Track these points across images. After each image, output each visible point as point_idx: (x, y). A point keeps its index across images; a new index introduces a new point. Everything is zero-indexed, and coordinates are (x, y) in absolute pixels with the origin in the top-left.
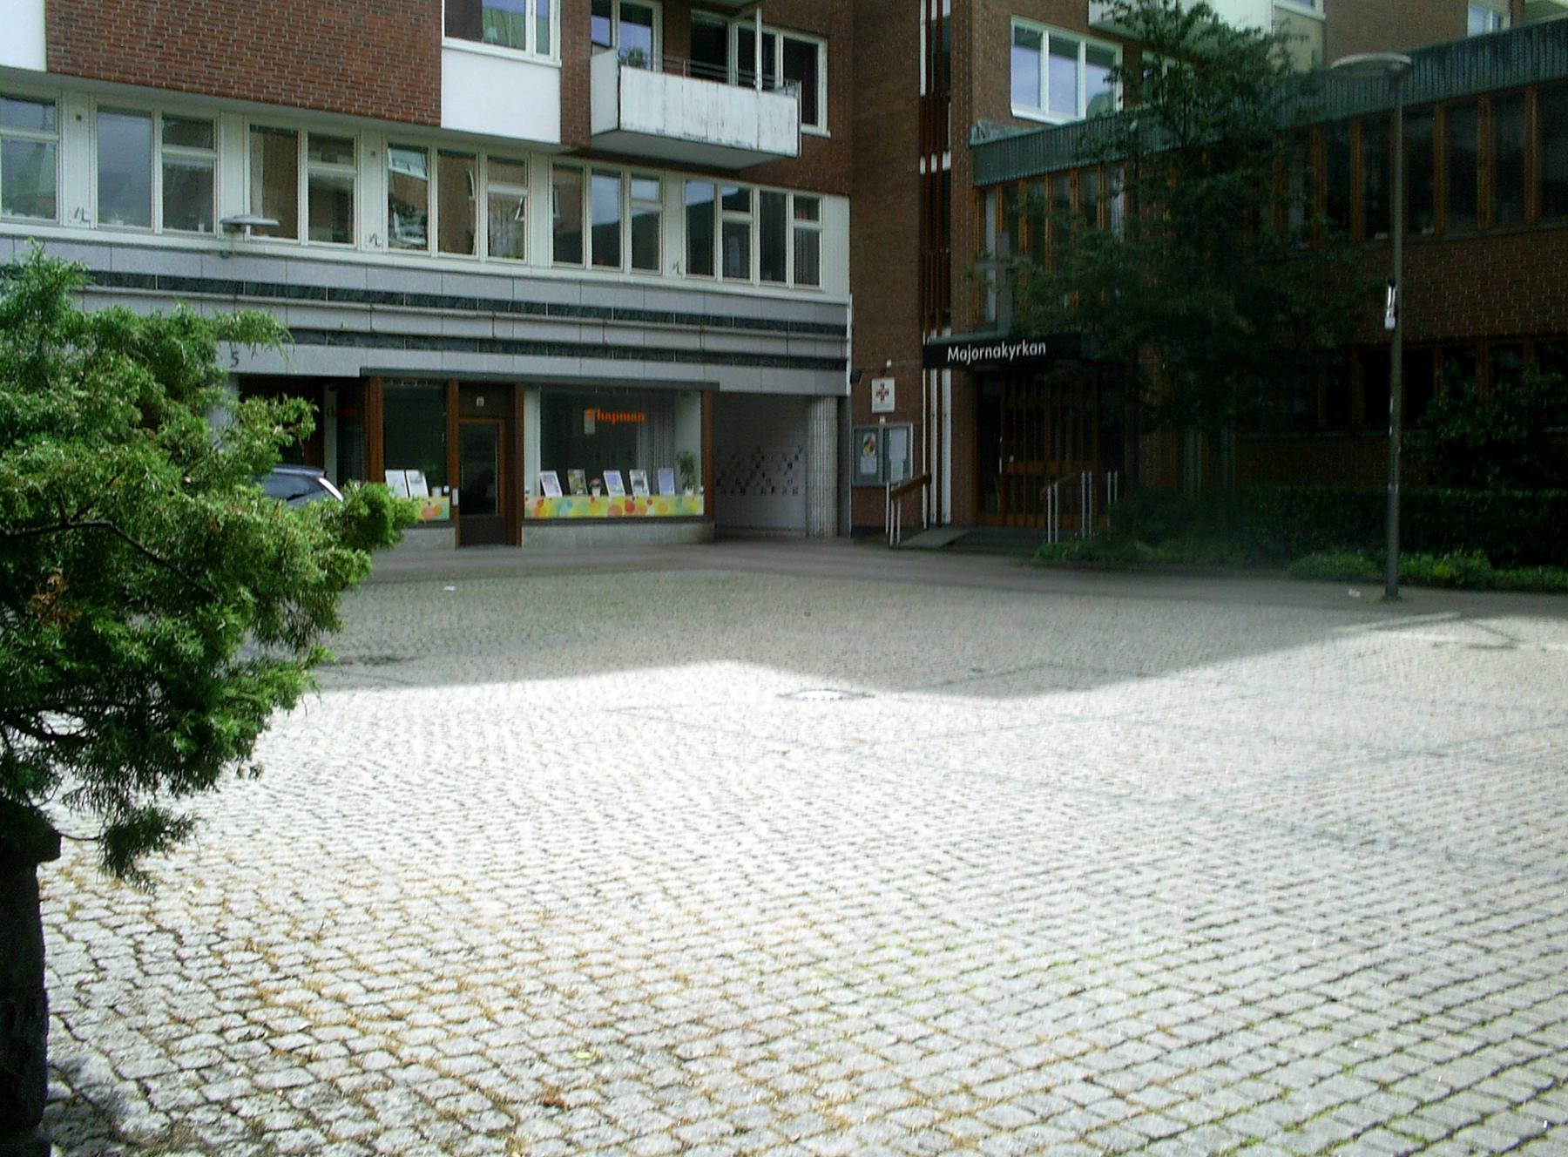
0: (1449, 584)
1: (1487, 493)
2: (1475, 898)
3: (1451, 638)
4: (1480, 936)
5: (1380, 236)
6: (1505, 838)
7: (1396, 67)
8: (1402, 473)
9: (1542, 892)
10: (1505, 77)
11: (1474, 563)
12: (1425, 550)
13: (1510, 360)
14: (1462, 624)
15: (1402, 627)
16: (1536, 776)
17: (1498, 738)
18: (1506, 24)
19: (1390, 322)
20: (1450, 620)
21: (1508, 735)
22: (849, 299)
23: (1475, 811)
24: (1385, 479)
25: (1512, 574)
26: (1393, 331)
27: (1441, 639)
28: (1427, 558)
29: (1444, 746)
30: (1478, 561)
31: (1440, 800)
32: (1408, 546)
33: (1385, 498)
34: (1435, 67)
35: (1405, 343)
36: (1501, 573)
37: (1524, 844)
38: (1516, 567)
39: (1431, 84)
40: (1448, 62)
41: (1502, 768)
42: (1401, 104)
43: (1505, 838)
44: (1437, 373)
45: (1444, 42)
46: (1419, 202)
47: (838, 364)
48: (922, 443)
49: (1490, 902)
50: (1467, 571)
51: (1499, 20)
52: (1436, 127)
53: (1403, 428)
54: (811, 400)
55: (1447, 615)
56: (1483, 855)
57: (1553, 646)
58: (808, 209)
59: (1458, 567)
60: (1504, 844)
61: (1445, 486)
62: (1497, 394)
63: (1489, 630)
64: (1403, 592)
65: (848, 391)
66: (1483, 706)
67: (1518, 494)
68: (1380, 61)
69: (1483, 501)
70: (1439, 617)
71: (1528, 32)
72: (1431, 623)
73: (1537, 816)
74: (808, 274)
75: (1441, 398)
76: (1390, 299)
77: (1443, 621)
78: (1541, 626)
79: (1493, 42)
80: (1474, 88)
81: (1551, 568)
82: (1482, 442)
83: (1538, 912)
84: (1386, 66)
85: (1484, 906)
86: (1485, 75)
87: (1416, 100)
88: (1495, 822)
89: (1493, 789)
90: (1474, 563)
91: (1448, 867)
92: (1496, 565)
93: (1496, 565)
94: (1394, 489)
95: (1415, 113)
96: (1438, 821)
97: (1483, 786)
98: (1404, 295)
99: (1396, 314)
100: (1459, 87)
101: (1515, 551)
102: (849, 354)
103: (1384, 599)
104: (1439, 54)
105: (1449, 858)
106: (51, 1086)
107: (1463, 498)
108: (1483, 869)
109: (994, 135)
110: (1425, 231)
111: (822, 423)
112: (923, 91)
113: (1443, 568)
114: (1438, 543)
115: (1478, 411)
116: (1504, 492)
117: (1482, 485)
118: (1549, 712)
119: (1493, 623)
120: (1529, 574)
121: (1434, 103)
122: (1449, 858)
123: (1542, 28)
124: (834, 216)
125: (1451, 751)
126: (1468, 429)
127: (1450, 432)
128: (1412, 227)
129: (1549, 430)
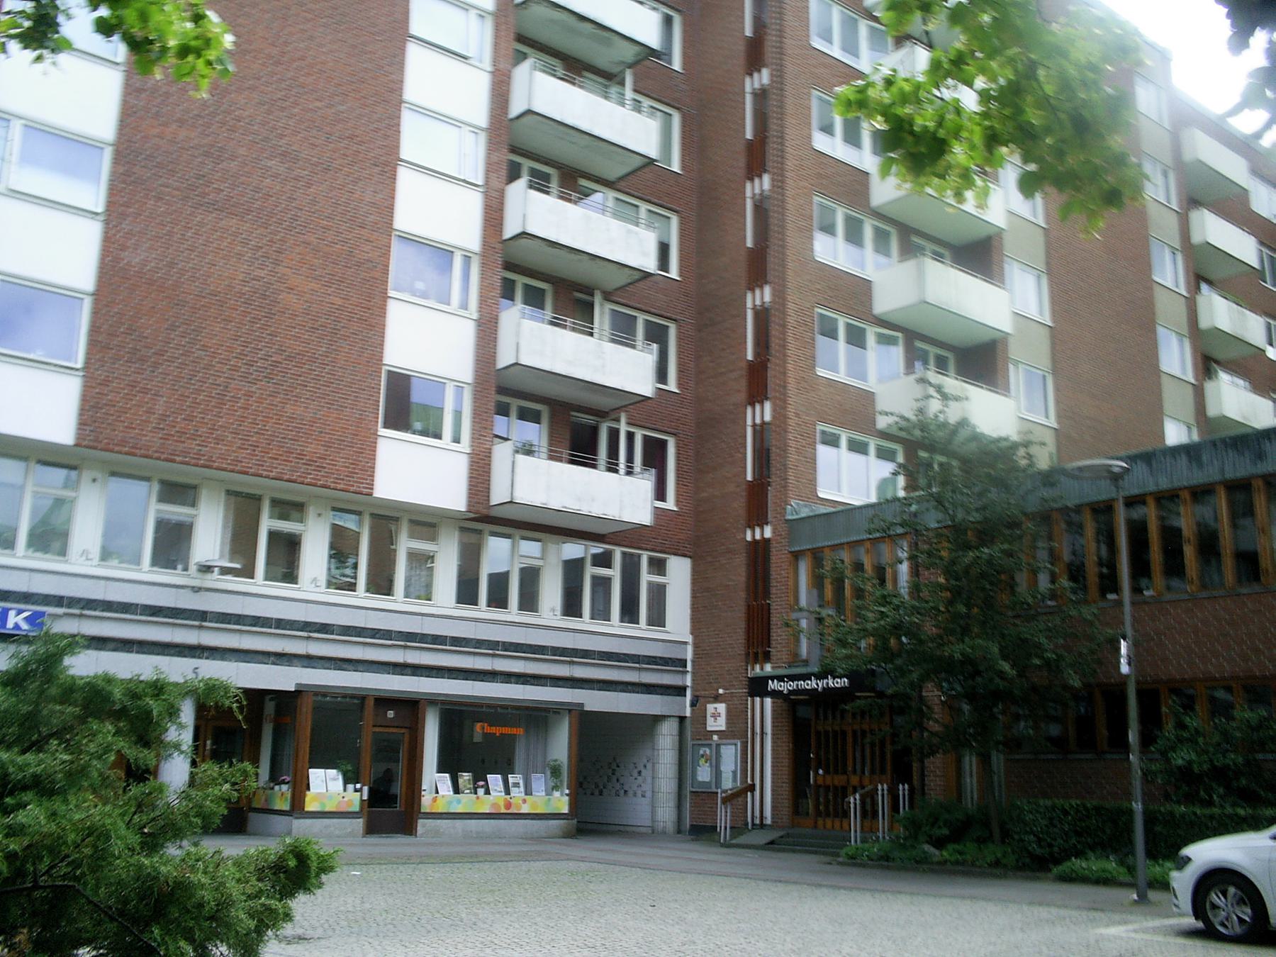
22: (689, 639)
47: (680, 691)
48: (747, 756)
54: (657, 719)
58: (658, 566)
65: (688, 713)
74: (657, 618)
102: (688, 681)
109: (805, 513)
111: (666, 736)
124: (679, 572)
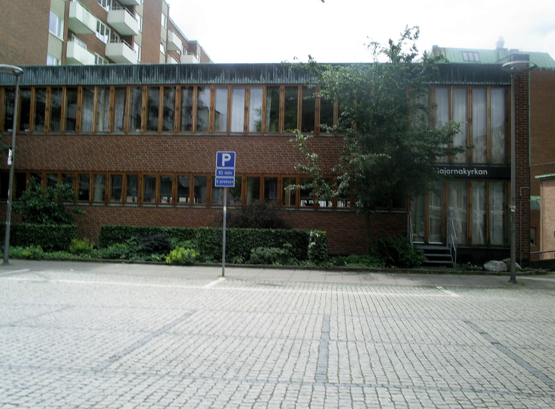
0: (28, 258)
1: (43, 225)
2: (17, 384)
3: (26, 279)
4: (17, 399)
5: (9, 130)
6: (32, 357)
7: (17, 71)
8: (12, 216)
9: (42, 377)
10: (56, 82)
11: (37, 250)
12: (20, 245)
13: (52, 178)
14: (31, 273)
15: (8, 275)
16: (47, 331)
17: (37, 317)
18: (60, 64)
19: (10, 162)
20: (26, 272)
21: (40, 315)
23: (23, 347)
24: (5, 219)
25: (50, 254)
26: (10, 166)
27: (22, 279)
28: (21, 248)
29: (16, 322)
30: (39, 250)
31: (10, 344)
32: (13, 244)
33: (5, 226)
34: (33, 74)
35: (15, 170)
36: (46, 254)
37: (39, 359)
38: (52, 252)
39: (30, 79)
40: (37, 73)
41: (36, 329)
42: (18, 84)
43: (32, 357)
44: (27, 181)
45: (37, 66)
46: (24, 119)
49: (22, 384)
50: (35, 253)
51: (58, 61)
52: (32, 95)
53: (13, 200)
55: (25, 270)
56: (23, 365)
57: (61, 281)
59: (31, 252)
60: (31, 359)
61: (28, 222)
62: (48, 191)
63: (40, 276)
64: (11, 261)
66: (33, 305)
67: (54, 226)
68: (11, 68)
69: (41, 228)
70: (21, 271)
71: (65, 68)
72: (19, 274)
73: (45, 347)
75: (28, 191)
76: (538, 177)
77: (24, 273)
78: (58, 273)
79: (54, 69)
80: (45, 84)
81: (63, 252)
82: (42, 207)
83: (40, 385)
84: (13, 70)
85: (20, 386)
86: (49, 80)
87: (25, 84)
88: (30, 351)
89: (31, 338)
90: (37, 250)
91: (9, 372)
92: (45, 250)
93: (45, 250)
94: (8, 223)
95: (24, 88)
96: (8, 353)
97: (28, 337)
98: (16, 153)
99: (12, 160)
100: (40, 82)
101: (52, 246)
103: (3, 264)
104: (35, 69)
105: (10, 368)
106: (430, 206)
107: (34, 227)
108: (22, 370)
110: (26, 130)
112: (536, 177)
113: (26, 252)
114: (25, 243)
115: (41, 196)
116: (49, 225)
117: (41, 222)
118: (56, 305)
119: (42, 273)
120: (56, 254)
121: (31, 86)
122: (10, 368)
123: (69, 67)
125: (18, 324)
126: (37, 203)
127: (30, 204)
128: (21, 128)
129: (65, 203)
